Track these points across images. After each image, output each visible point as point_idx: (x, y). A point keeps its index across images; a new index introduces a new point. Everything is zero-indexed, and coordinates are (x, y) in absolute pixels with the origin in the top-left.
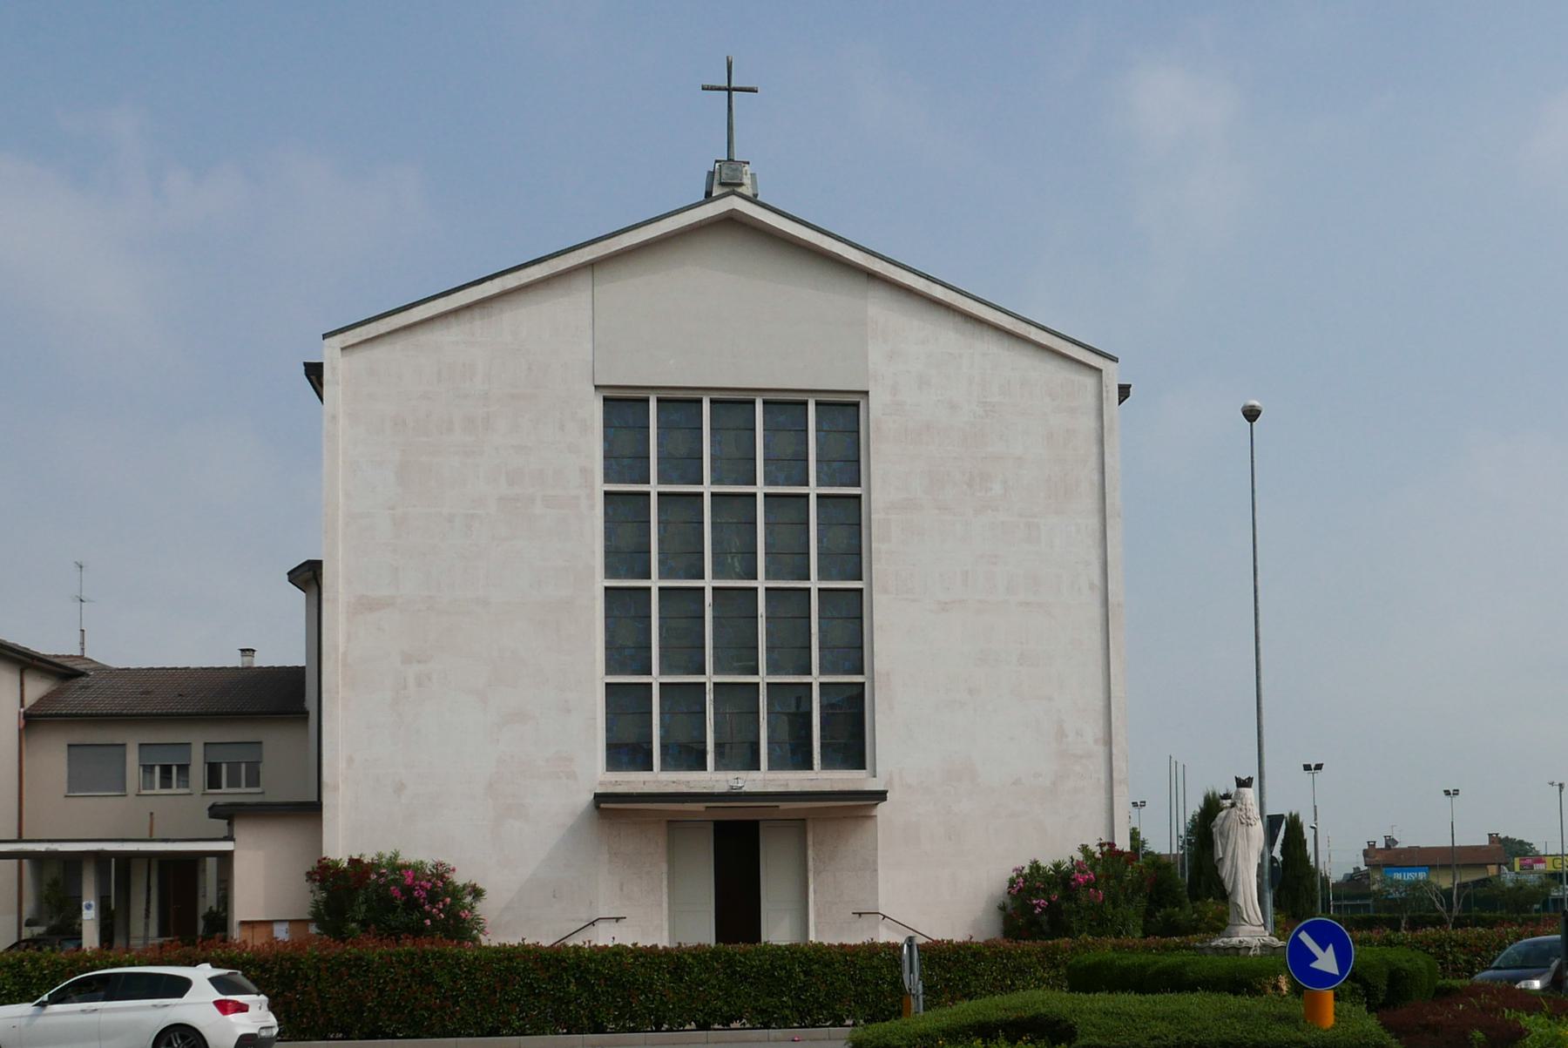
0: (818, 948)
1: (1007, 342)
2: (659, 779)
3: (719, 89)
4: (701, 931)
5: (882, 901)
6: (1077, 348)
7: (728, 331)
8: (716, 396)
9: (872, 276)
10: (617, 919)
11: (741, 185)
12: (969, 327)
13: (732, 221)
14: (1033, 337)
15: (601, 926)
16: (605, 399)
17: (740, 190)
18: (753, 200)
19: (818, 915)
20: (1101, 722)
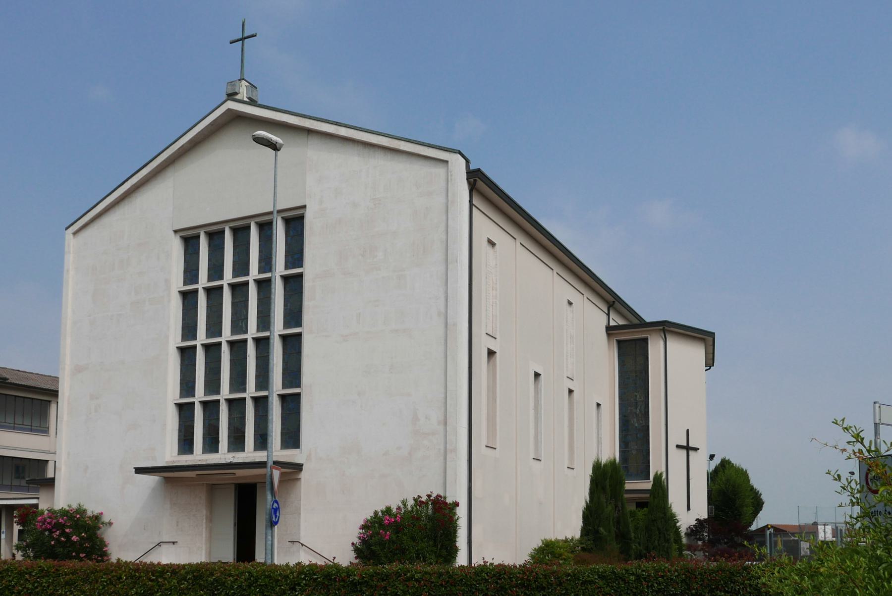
0: (484, 569)
1: (389, 156)
2: (199, 456)
3: (243, 45)
4: (227, 553)
5: (302, 533)
6: (431, 149)
7: (231, 183)
8: (232, 224)
9: (309, 132)
10: (174, 543)
11: (236, 94)
12: (366, 151)
13: (234, 119)
14: (402, 148)
15: (164, 546)
16: (619, 342)
17: (238, 97)
18: (252, 102)
19: (279, 542)
20: (443, 409)
